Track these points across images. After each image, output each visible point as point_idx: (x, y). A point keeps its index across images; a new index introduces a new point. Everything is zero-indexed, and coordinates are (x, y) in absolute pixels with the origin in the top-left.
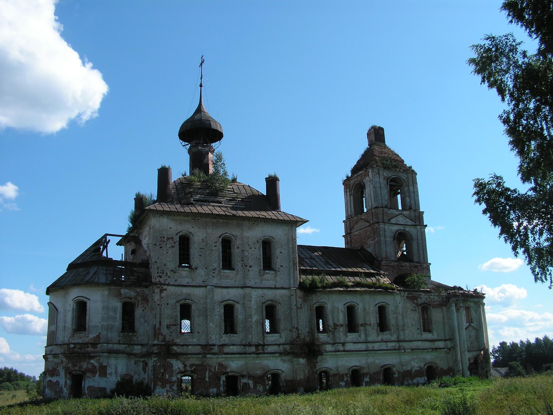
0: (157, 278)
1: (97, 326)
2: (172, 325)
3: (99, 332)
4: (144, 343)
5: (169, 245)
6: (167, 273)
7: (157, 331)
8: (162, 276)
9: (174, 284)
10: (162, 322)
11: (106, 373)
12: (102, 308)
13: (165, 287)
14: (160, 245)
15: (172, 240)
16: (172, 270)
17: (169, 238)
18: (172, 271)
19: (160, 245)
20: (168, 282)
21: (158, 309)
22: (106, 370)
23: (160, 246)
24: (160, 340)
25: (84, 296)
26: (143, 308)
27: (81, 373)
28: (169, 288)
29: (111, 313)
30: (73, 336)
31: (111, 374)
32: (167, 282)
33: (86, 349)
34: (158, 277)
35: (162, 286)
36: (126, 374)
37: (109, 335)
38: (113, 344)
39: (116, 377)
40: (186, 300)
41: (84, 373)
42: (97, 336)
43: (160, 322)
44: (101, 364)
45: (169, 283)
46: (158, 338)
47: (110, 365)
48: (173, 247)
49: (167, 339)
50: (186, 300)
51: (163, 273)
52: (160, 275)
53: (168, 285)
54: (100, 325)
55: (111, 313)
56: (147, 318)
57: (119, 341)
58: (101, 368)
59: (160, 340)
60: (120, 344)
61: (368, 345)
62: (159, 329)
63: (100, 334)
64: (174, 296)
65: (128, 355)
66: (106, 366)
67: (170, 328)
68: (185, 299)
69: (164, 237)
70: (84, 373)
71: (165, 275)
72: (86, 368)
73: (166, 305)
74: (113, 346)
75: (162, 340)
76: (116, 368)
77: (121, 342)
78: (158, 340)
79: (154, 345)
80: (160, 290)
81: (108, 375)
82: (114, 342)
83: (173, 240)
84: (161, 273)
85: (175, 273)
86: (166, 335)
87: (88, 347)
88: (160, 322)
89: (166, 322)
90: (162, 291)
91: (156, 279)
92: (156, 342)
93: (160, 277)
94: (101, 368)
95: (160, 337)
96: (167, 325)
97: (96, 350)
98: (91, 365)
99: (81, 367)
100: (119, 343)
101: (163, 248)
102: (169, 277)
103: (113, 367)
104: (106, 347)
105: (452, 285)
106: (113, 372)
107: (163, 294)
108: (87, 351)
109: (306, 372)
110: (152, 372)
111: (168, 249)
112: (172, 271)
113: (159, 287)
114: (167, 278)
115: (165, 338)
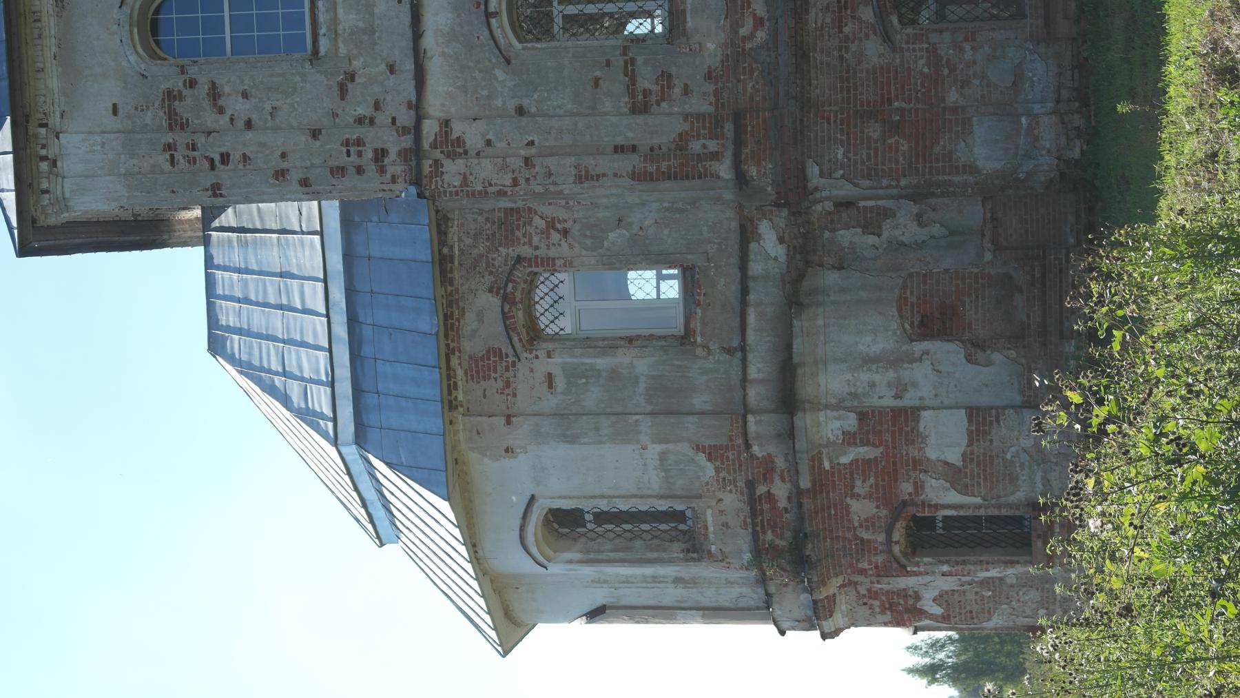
0: (388, 176)
1: (661, 460)
2: (633, 80)
3: (691, 453)
4: (734, 225)
5: (210, 119)
6: (360, 121)
7: (664, 165)
8: (379, 145)
9: (411, 75)
10: (620, 140)
11: (898, 413)
12: (571, 442)
13: (430, 128)
14: (213, 167)
15: (180, 97)
16: (336, 92)
17: (172, 115)
18: (343, 91)
19: (213, 167)
20: (404, 109)
21: (552, 162)
22: (880, 413)
23: (217, 163)
24: (712, 145)
25: (517, 522)
26: (555, 236)
27: (900, 526)
28: (436, 103)
29: (593, 397)
30: (722, 559)
31: (900, 389)
32: (406, 118)
33: (782, 504)
34: (382, 170)
35: (426, 146)
36: (900, 311)
37: (700, 401)
38: (744, 380)
39: (912, 360)
40: (492, 9)
41: (898, 509)
42: (710, 460)
43: (618, 149)
44: (850, 439)
45: (410, 103)
46: (700, 158)
47: (854, 395)
48: (214, 93)
49: (705, 107)
50: (492, 9)
51: (359, 142)
52: (370, 155)
53: (417, 106)
54: (655, 449)
55: (593, 397)
56: (602, 214)
57: (730, 351)
58: (871, 437)
59: (712, 145)
60: (743, 349)
61: (754, 435)
62: (654, 153)
63: (699, 448)
64: (477, 74)
65: (800, 305)
66: (862, 416)
67: (646, 93)
68: (488, 15)
69: (170, 147)
70: (898, 509)
71: (368, 133)
72: (878, 499)
73: (524, 120)
74: (755, 381)
75: (712, 136)
76: (869, 361)
77: (735, 344)
78: (715, 156)
79: (741, 179)
80: (452, 156)
81: (908, 401)
82: (735, 374)
83: (180, 97)
84: (360, 154)
85: (351, 77)
86: (686, 117)
87: (770, 497)
88: (618, 149)
89: (629, 129)
90: (452, 146)
91: (394, 180)
92: (724, 170)
93: (381, 154)
94: (871, 437)
95: (696, 146)
96: (634, 111)
97: (780, 463)
98: (858, 483)
99: (868, 523)
100: (739, 354)
101: (224, 150)
102: (377, 106)
103: (865, 377)
104: (765, 417)
105: (852, 628)
106: (891, 375)
107: (473, 140)
108: (789, 499)
109: (710, 520)
110: (885, 182)
111: (232, 120)
112: (343, 91)
113: (437, 163)
114: (383, 118)
115: (700, 117)
